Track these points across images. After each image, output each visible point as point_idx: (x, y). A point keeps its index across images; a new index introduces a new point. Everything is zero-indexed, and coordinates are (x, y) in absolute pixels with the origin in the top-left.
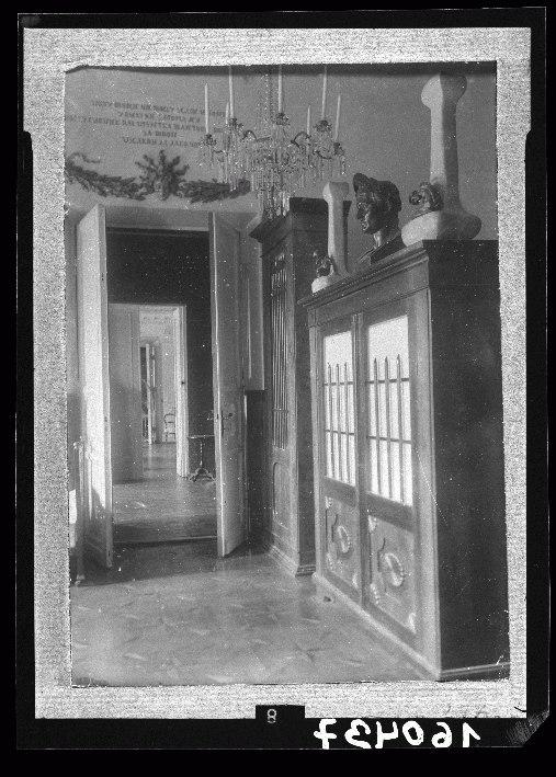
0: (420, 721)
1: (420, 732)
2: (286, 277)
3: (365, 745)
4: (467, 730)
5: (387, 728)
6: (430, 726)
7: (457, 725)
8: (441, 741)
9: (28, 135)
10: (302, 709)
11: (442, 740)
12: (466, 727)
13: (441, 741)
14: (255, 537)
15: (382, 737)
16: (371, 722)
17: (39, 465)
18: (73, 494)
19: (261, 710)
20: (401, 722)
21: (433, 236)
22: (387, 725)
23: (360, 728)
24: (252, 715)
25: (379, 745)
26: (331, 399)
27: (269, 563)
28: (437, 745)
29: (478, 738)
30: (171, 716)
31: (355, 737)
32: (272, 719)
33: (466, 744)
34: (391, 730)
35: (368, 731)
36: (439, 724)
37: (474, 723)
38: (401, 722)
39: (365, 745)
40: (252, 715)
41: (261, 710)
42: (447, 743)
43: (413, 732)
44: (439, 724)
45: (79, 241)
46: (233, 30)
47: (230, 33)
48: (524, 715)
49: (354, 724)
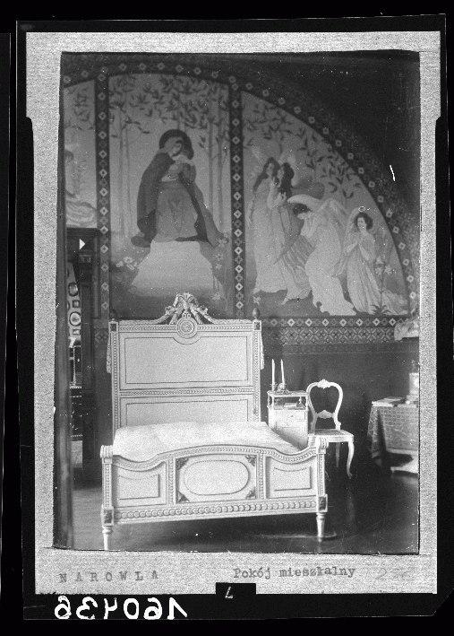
4: (173, 603)
6: (143, 600)
7: (164, 599)
10: (254, 585)
13: (152, 614)
14: (159, 496)
16: (99, 598)
19: (221, 587)
21: (260, 591)
22: (111, 599)
23: (89, 603)
24: (212, 590)
25: (106, 617)
27: (101, 491)
29: (185, 615)
31: (82, 613)
33: (171, 617)
35: (95, 605)
36: (150, 600)
37: (179, 598)
38: (121, 598)
40: (212, 590)
41: (218, 585)
42: (158, 615)
44: (150, 600)
46: (63, 33)
49: (85, 600)
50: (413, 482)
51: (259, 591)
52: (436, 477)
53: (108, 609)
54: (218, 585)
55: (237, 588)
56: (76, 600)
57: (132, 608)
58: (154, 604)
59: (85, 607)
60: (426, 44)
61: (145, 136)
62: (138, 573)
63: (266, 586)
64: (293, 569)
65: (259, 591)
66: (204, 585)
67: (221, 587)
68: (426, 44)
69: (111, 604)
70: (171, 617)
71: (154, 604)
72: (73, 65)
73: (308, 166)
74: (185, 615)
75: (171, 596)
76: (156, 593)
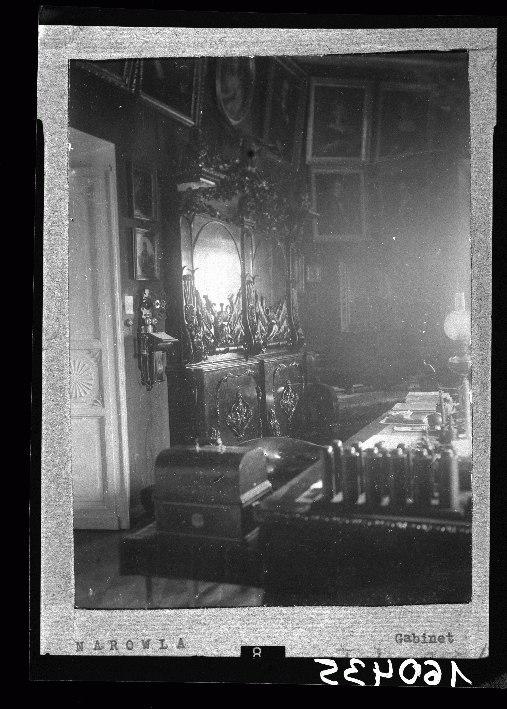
1: (418, 668)
2: (446, 429)
3: (336, 683)
8: (431, 679)
9: (40, 122)
10: (282, 649)
11: (435, 678)
13: (431, 679)
15: (379, 674)
16: (369, 662)
17: (54, 558)
18: (268, 484)
20: (397, 662)
23: (356, 665)
24: (237, 654)
25: (377, 684)
28: (430, 683)
31: (349, 676)
32: (257, 656)
33: (453, 685)
34: (387, 671)
36: (316, 661)
37: (461, 663)
38: (397, 662)
39: (336, 683)
40: (237, 654)
41: (244, 649)
42: (436, 682)
43: (409, 672)
45: (101, 527)
48: (42, 653)
51: (287, 655)
52: (488, 533)
54: (244, 649)
56: (343, 663)
59: (354, 670)
60: (480, 43)
62: (162, 641)
64: (438, 634)
65: (287, 655)
67: (246, 650)
68: (480, 43)
69: (384, 669)
70: (453, 685)
71: (432, 668)
72: (81, 73)
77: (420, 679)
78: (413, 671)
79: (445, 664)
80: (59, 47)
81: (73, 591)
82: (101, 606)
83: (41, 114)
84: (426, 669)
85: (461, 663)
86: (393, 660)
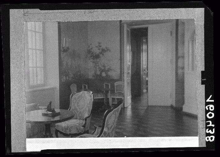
0: (206, 105)
1: (210, 113)
3: (214, 130)
4: (208, 100)
5: (209, 123)
8: (212, 108)
9: (42, 151)
10: (202, 71)
12: (207, 101)
13: (212, 108)
16: (207, 128)
20: (207, 119)
23: (208, 131)
24: (204, 86)
25: (213, 126)
26: (143, 61)
29: (211, 96)
30: (203, 55)
31: (212, 131)
33: (213, 101)
37: (206, 99)
38: (207, 119)
39: (214, 130)
40: (204, 86)
41: (202, 84)
42: (213, 106)
43: (210, 115)
47: (12, 144)
50: (98, 130)
51: (204, 70)
53: (211, 125)
54: (202, 84)
55: (203, 77)
57: (210, 115)
58: (208, 107)
61: (170, 34)
63: (201, 66)
66: (201, 89)
70: (213, 101)
73: (110, 51)
74: (211, 96)
75: (206, 122)
76: (205, 131)
77: (212, 111)
78: (211, 114)
79: (207, 104)
80: (196, 16)
81: (4, 71)
82: (62, 35)
83: (39, 150)
84: (209, 111)
85: (206, 99)
86: (206, 121)
